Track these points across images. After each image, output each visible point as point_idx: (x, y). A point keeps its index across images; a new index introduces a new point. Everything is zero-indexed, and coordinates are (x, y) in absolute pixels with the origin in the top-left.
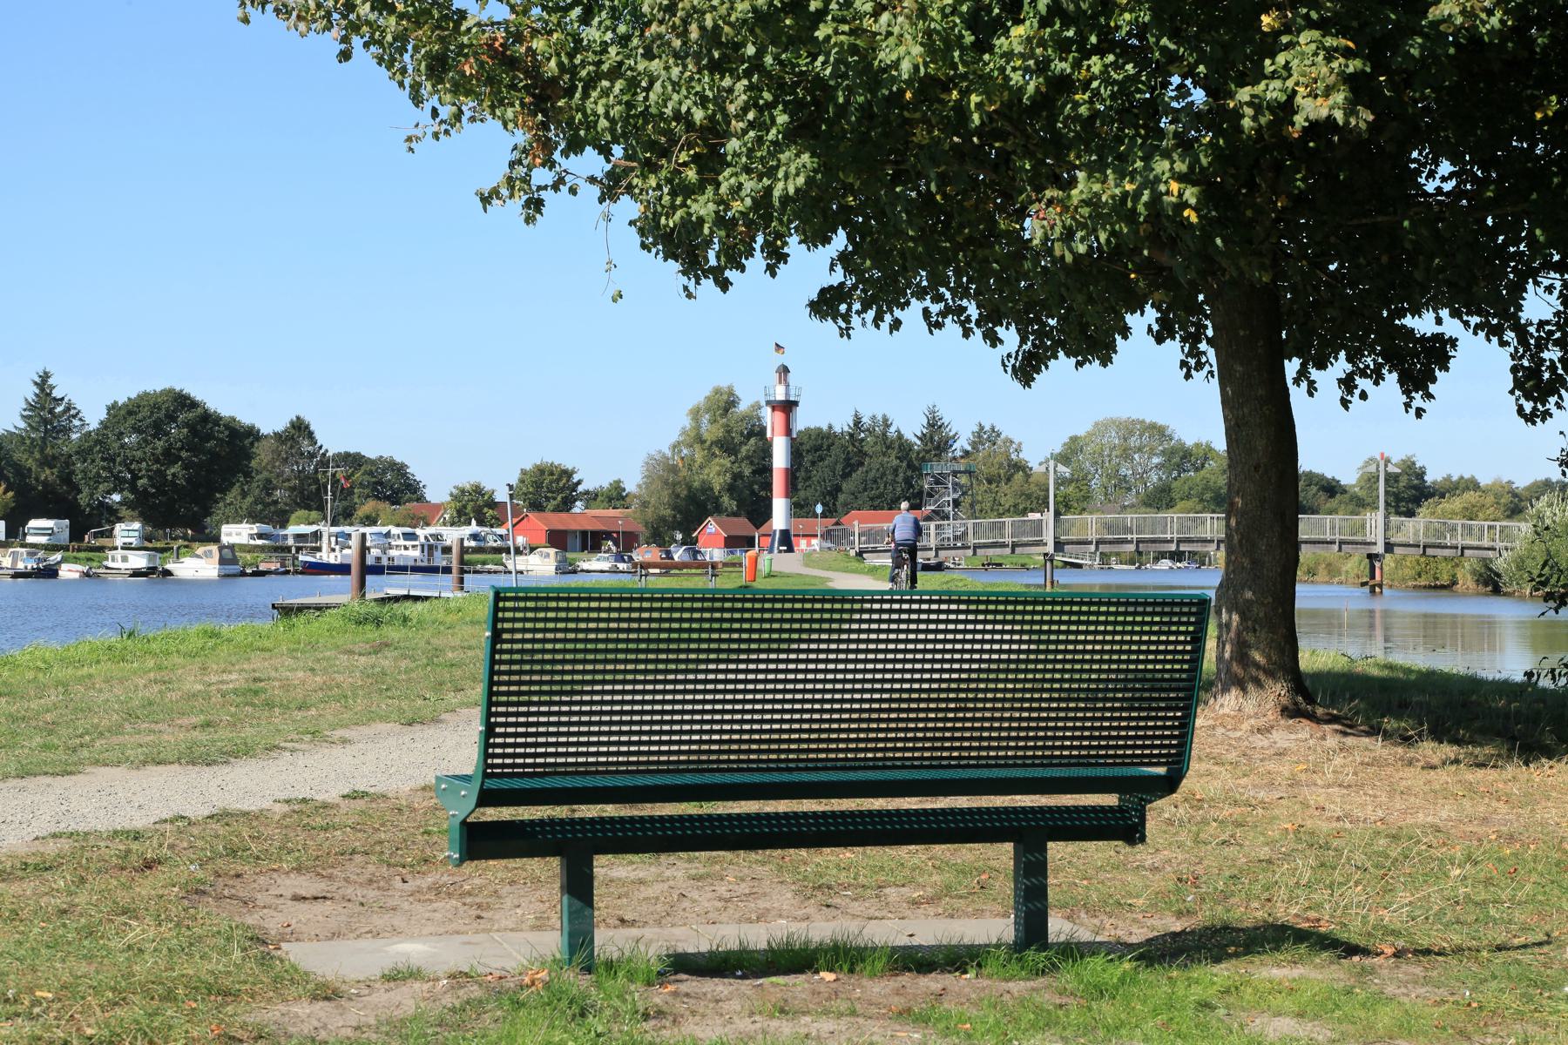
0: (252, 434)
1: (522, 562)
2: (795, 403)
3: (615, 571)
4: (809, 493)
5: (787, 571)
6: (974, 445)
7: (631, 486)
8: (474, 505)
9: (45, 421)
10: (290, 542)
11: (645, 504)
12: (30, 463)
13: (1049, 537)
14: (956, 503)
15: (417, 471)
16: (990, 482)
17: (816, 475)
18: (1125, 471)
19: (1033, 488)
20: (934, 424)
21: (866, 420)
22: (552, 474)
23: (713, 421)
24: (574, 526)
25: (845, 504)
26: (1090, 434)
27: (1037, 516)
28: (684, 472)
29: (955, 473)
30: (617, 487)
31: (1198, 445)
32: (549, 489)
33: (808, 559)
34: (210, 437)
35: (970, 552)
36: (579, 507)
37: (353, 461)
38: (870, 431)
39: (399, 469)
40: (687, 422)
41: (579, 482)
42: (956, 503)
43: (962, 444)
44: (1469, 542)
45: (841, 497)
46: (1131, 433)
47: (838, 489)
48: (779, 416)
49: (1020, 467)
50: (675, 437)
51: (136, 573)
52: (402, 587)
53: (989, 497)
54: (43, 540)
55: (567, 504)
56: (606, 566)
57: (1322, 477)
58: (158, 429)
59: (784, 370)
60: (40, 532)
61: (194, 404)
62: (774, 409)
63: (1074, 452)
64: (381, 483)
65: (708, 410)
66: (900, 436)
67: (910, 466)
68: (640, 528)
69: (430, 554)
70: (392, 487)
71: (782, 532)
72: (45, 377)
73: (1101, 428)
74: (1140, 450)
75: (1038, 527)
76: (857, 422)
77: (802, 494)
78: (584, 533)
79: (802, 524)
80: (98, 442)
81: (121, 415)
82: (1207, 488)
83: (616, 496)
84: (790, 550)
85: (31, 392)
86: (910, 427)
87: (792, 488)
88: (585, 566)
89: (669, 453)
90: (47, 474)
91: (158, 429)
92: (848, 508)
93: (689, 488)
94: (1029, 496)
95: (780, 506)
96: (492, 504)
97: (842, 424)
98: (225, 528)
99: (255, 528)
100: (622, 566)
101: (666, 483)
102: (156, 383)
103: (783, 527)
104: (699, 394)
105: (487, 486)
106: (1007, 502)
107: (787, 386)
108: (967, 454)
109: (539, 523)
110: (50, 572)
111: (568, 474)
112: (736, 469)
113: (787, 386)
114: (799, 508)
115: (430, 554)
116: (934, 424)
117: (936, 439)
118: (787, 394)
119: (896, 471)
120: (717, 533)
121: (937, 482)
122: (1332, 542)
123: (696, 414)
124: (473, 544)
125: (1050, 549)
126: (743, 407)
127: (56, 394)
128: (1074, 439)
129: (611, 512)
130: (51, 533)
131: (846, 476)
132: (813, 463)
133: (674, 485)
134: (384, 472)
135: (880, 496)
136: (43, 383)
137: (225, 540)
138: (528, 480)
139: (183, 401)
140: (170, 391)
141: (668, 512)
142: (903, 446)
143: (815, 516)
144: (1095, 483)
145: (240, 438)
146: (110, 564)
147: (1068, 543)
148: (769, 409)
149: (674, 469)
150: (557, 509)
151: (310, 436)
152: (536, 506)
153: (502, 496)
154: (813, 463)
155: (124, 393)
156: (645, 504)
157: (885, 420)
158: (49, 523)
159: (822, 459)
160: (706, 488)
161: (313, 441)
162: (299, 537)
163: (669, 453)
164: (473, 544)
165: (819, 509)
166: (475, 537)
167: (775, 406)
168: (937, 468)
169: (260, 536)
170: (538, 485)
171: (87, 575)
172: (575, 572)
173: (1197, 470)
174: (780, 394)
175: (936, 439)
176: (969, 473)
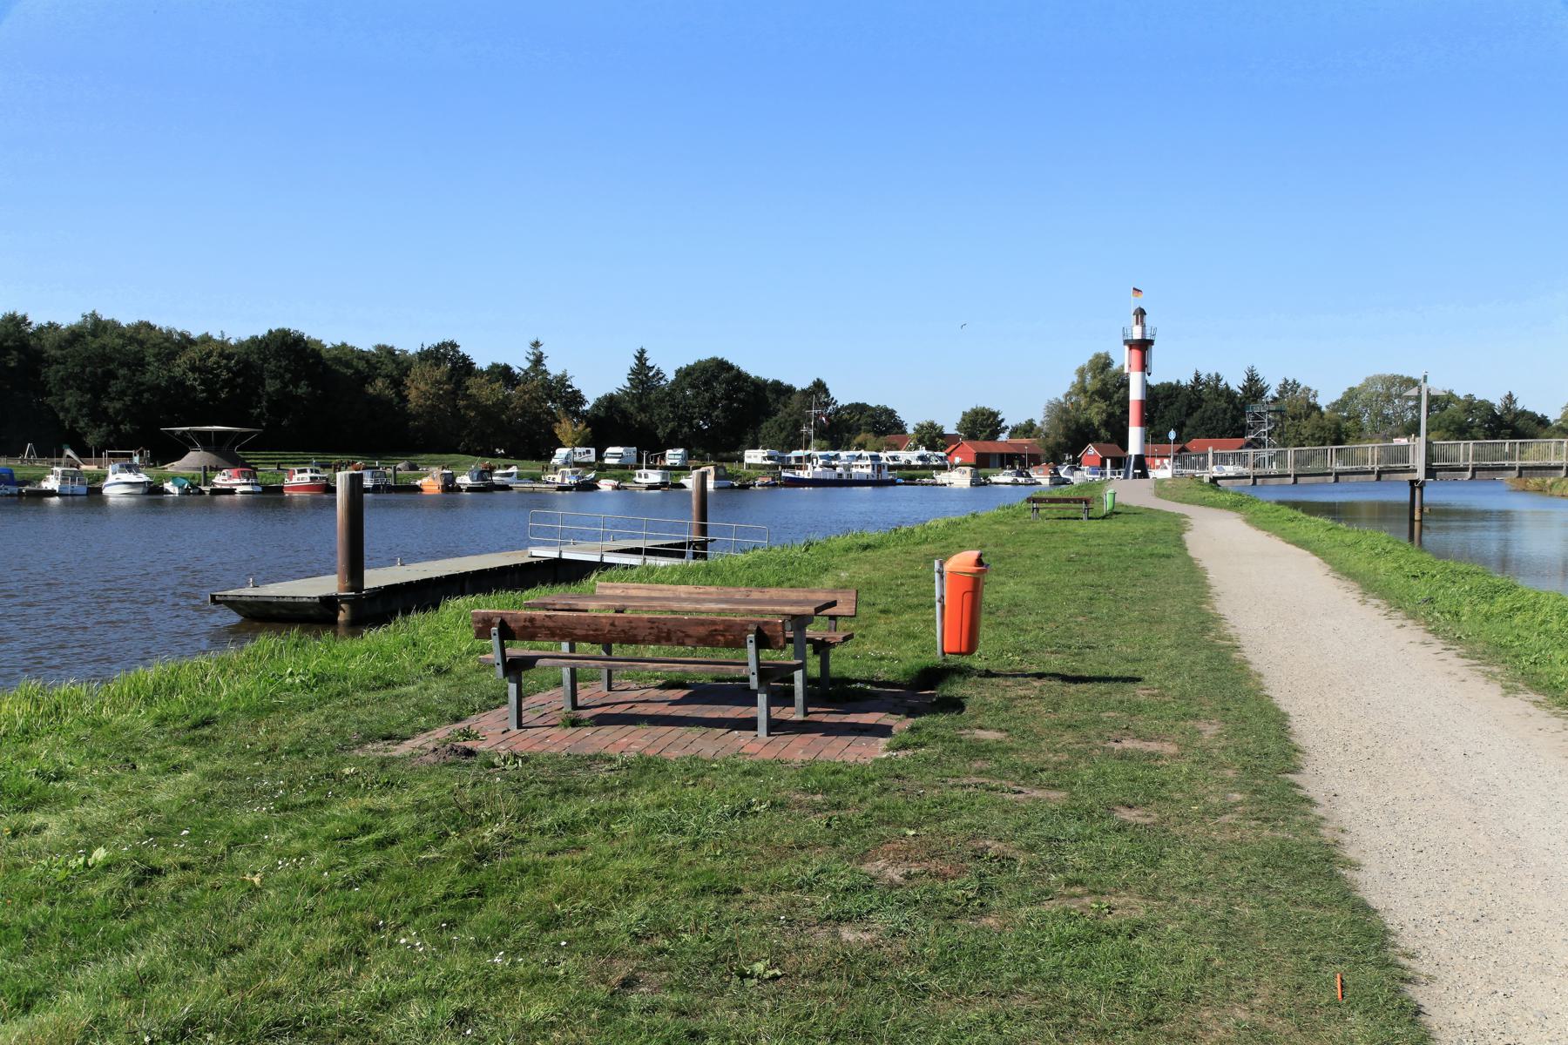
0: (790, 390)
1: (942, 477)
2: (1151, 342)
3: (1015, 483)
5: (1134, 504)
6: (1280, 393)
7: (1039, 419)
8: (931, 437)
9: (642, 382)
10: (793, 462)
11: (1047, 435)
12: (632, 409)
13: (1419, 462)
15: (902, 415)
17: (1168, 415)
20: (1252, 379)
23: (1094, 377)
24: (994, 451)
27: (1404, 441)
28: (1073, 413)
32: (982, 424)
33: (1161, 488)
34: (740, 390)
36: (1003, 437)
37: (860, 408)
38: (1207, 385)
39: (891, 414)
40: (1075, 379)
43: (1272, 392)
46: (1393, 385)
48: (1136, 353)
50: (1066, 388)
51: (651, 487)
52: (592, 551)
53: (1293, 430)
54: (615, 461)
55: (994, 435)
56: (1009, 479)
58: (707, 384)
59: (1141, 313)
60: (614, 456)
61: (730, 368)
62: (1131, 348)
63: (1351, 398)
65: (1091, 369)
67: (1235, 407)
68: (1042, 451)
69: (879, 471)
70: (880, 425)
72: (642, 352)
73: (1371, 381)
75: (1403, 454)
76: (1197, 378)
77: (1158, 428)
78: (1002, 455)
79: (1156, 448)
80: (668, 394)
81: (685, 374)
82: (1453, 422)
83: (1028, 429)
84: (1144, 475)
85: (633, 362)
86: (1235, 381)
87: (1146, 422)
88: (994, 479)
90: (642, 417)
91: (707, 384)
92: (1190, 437)
93: (1077, 423)
94: (1323, 428)
95: (1135, 435)
96: (942, 435)
97: (1186, 379)
98: (747, 453)
99: (766, 453)
100: (1021, 480)
102: (705, 355)
104: (1085, 359)
106: (1306, 432)
107: (1144, 326)
108: (1275, 399)
109: (970, 449)
110: (590, 486)
111: (995, 415)
112: (1110, 410)
113: (1144, 326)
114: (1154, 435)
115: (879, 471)
116: (1252, 379)
117: (1254, 389)
118: (1143, 333)
122: (1466, 469)
123: (1081, 372)
125: (1420, 475)
126: (1115, 366)
127: (649, 363)
128: (1351, 389)
129: (1025, 441)
130: (622, 457)
131: (1188, 415)
136: (641, 357)
137: (747, 460)
139: (722, 366)
140: (714, 359)
141: (1062, 440)
142: (1229, 394)
143: (1168, 441)
145: (781, 391)
146: (637, 479)
149: (1066, 411)
150: (987, 439)
151: (826, 391)
152: (972, 436)
153: (910, 430)
155: (689, 359)
156: (1047, 435)
157: (1217, 376)
158: (619, 450)
160: (1089, 423)
161: (828, 395)
162: (799, 459)
165: (1172, 435)
166: (921, 458)
167: (1132, 344)
168: (1257, 408)
169: (770, 458)
170: (974, 422)
171: (617, 488)
173: (1442, 410)
174: (1137, 334)
175: (1254, 389)
176: (1279, 411)
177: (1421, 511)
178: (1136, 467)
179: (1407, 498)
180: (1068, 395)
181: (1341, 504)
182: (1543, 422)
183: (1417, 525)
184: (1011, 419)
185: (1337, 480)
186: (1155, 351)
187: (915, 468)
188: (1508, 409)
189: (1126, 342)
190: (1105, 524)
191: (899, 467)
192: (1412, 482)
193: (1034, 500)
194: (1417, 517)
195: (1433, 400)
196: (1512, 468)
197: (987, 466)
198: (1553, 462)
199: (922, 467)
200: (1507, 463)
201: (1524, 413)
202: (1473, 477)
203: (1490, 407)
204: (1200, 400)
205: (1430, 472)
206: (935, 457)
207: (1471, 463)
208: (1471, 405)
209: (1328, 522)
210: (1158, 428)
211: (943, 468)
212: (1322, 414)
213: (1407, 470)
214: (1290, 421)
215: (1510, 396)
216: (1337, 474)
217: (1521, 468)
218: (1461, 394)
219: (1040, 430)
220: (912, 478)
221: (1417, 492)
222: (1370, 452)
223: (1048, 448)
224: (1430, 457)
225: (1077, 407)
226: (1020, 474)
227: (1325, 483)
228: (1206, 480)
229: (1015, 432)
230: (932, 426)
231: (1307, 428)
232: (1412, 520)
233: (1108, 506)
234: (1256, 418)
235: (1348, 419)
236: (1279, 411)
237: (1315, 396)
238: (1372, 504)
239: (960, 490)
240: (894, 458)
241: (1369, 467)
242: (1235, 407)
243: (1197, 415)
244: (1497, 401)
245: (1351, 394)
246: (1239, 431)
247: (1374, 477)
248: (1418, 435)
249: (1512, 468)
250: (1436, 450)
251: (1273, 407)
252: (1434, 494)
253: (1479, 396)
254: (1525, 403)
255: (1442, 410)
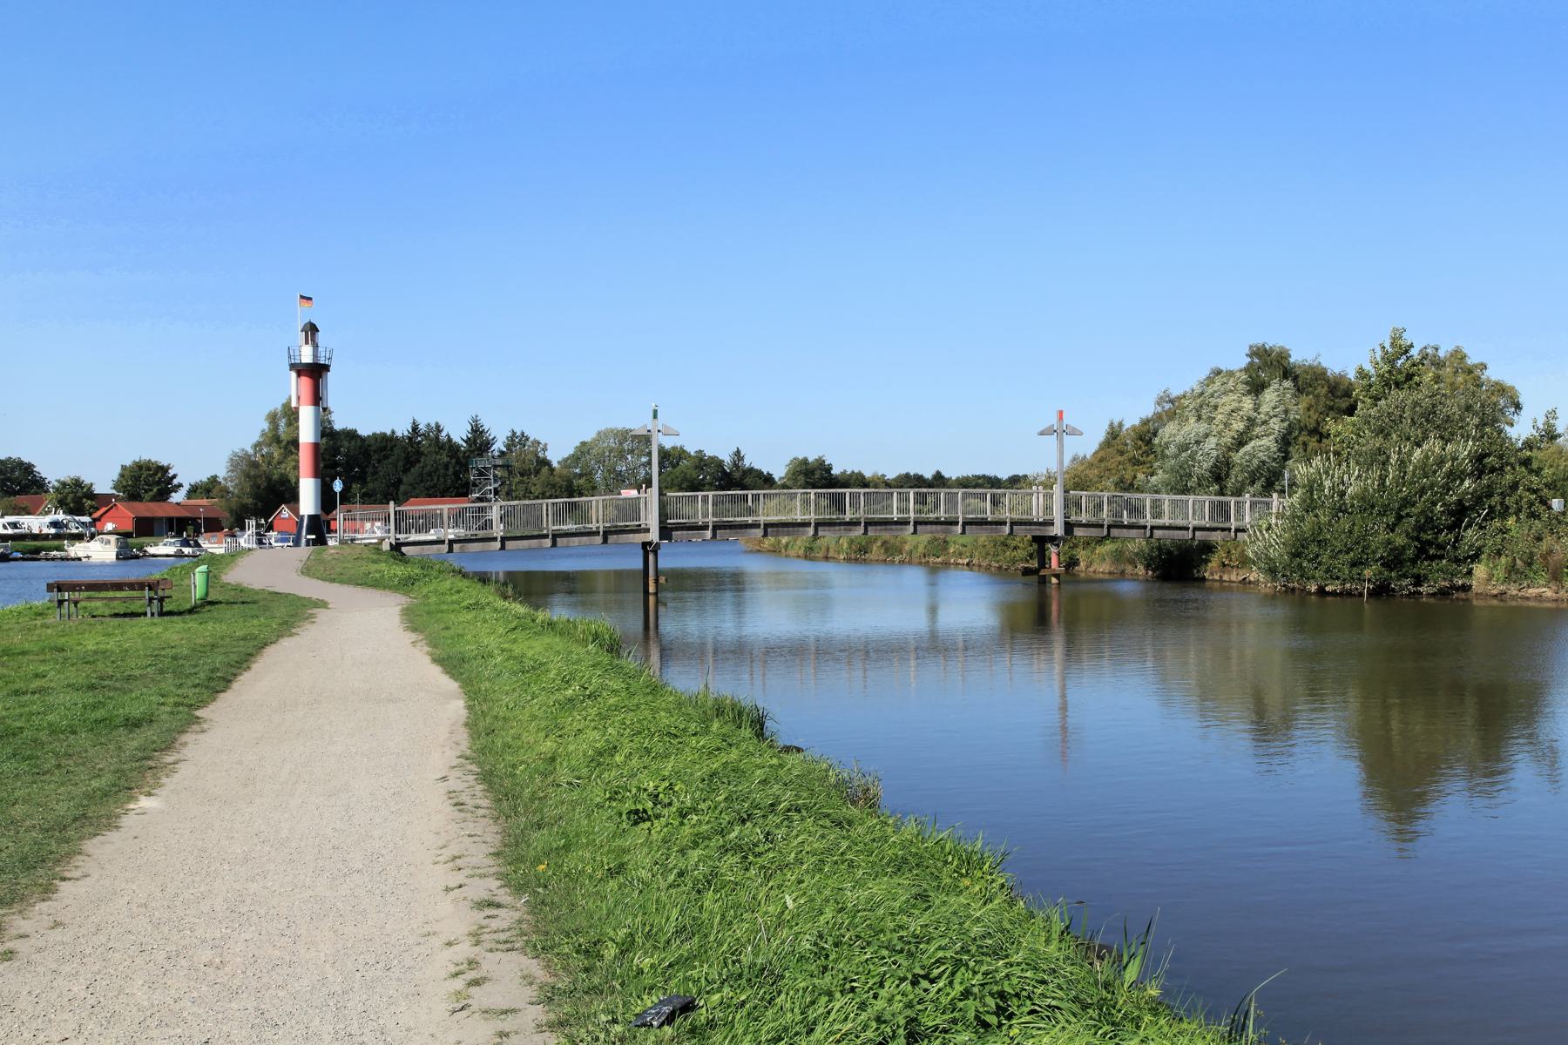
1: (77, 549)
2: (326, 368)
3: (179, 555)
4: (377, 484)
6: (508, 447)
7: (222, 472)
8: (78, 498)
13: (652, 520)
14: (496, 492)
16: (522, 475)
17: (382, 471)
18: (622, 467)
19: (557, 479)
20: (477, 431)
21: (422, 427)
22: (149, 469)
25: (405, 493)
26: (595, 440)
27: (633, 493)
28: (264, 467)
29: (495, 467)
30: (214, 480)
31: (674, 448)
35: (548, 542)
36: (178, 497)
38: (426, 436)
39: (28, 468)
40: (266, 426)
41: (174, 476)
42: (496, 492)
43: (499, 446)
44: (1159, 522)
45: (402, 488)
47: (400, 481)
48: (306, 382)
49: (545, 463)
53: (522, 487)
56: (171, 550)
57: (760, 473)
59: (311, 330)
62: (299, 374)
64: (9, 479)
66: (450, 440)
67: (458, 462)
71: (310, 517)
73: (603, 436)
74: (631, 452)
75: (633, 508)
76: (415, 428)
77: (370, 486)
78: (170, 520)
82: (685, 479)
86: (458, 432)
88: (151, 550)
89: (251, 451)
93: (269, 479)
94: (554, 486)
96: (91, 495)
97: (403, 430)
100: (187, 550)
101: (248, 476)
103: (312, 512)
105: (86, 480)
106: (537, 490)
107: (316, 346)
108: (502, 453)
111: (164, 470)
113: (316, 346)
116: (477, 431)
117: (479, 441)
118: (315, 355)
119: (446, 466)
120: (290, 518)
121: (481, 474)
122: (705, 527)
124: (53, 531)
125: (653, 536)
129: (205, 502)
131: (406, 471)
132: (379, 461)
133: (256, 477)
134: (13, 470)
135: (434, 486)
138: (127, 473)
142: (451, 447)
144: (598, 476)
147: (677, 529)
148: (294, 374)
149: (255, 465)
150: (153, 499)
152: (134, 496)
154: (379, 461)
157: (438, 426)
159: (386, 457)
163: (251, 451)
164: (53, 531)
166: (54, 524)
167: (300, 370)
170: (137, 479)
172: (137, 557)
173: (674, 466)
174: (307, 357)
176: (506, 467)
177: (657, 581)
178: (309, 532)
179: (640, 565)
180: (257, 445)
181: (578, 572)
182: (768, 481)
183: (652, 599)
184: (188, 473)
185: (554, 544)
186: (331, 378)
187: (46, 537)
188: (735, 465)
189: (293, 366)
190: (192, 623)
191: (22, 537)
192: (645, 545)
193: (60, 587)
194: (652, 589)
195: (665, 455)
196: (755, 525)
197: (151, 534)
198: (799, 518)
199: (57, 537)
200: (750, 520)
201: (751, 470)
202: (714, 536)
203: (720, 464)
204: (419, 453)
205: (666, 532)
206: (74, 524)
207: (711, 519)
208: (702, 462)
209: (520, 609)
210: (370, 486)
211: (79, 537)
212: (552, 470)
213: (638, 530)
214: (519, 478)
215: (738, 452)
216: (555, 536)
217: (767, 526)
218: (691, 450)
219: (225, 491)
220: (37, 551)
221: (651, 557)
222: (598, 509)
223: (231, 511)
224: (663, 516)
225: (268, 458)
226: (186, 543)
227: (540, 548)
228: (386, 547)
229: (194, 491)
230: (77, 483)
231: (537, 484)
232: (646, 592)
233: (199, 591)
234: (481, 474)
235: (581, 476)
236: (506, 467)
237: (545, 450)
238: (608, 573)
239: (103, 565)
240: (14, 525)
241: (593, 526)
242: (458, 462)
243: (415, 470)
244: (726, 457)
245: (583, 449)
246: (461, 489)
247: (599, 539)
248: (649, 485)
249: (755, 525)
250: (670, 509)
251: (499, 462)
252: (672, 558)
253: (709, 453)
254: (752, 460)
255: (674, 466)
